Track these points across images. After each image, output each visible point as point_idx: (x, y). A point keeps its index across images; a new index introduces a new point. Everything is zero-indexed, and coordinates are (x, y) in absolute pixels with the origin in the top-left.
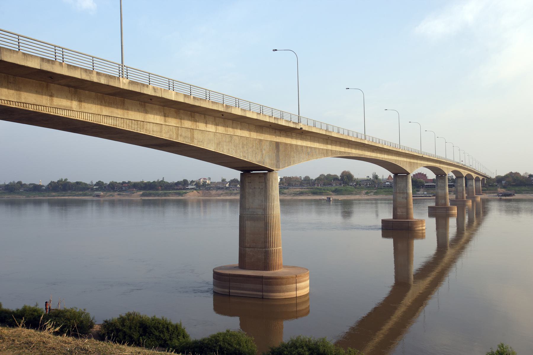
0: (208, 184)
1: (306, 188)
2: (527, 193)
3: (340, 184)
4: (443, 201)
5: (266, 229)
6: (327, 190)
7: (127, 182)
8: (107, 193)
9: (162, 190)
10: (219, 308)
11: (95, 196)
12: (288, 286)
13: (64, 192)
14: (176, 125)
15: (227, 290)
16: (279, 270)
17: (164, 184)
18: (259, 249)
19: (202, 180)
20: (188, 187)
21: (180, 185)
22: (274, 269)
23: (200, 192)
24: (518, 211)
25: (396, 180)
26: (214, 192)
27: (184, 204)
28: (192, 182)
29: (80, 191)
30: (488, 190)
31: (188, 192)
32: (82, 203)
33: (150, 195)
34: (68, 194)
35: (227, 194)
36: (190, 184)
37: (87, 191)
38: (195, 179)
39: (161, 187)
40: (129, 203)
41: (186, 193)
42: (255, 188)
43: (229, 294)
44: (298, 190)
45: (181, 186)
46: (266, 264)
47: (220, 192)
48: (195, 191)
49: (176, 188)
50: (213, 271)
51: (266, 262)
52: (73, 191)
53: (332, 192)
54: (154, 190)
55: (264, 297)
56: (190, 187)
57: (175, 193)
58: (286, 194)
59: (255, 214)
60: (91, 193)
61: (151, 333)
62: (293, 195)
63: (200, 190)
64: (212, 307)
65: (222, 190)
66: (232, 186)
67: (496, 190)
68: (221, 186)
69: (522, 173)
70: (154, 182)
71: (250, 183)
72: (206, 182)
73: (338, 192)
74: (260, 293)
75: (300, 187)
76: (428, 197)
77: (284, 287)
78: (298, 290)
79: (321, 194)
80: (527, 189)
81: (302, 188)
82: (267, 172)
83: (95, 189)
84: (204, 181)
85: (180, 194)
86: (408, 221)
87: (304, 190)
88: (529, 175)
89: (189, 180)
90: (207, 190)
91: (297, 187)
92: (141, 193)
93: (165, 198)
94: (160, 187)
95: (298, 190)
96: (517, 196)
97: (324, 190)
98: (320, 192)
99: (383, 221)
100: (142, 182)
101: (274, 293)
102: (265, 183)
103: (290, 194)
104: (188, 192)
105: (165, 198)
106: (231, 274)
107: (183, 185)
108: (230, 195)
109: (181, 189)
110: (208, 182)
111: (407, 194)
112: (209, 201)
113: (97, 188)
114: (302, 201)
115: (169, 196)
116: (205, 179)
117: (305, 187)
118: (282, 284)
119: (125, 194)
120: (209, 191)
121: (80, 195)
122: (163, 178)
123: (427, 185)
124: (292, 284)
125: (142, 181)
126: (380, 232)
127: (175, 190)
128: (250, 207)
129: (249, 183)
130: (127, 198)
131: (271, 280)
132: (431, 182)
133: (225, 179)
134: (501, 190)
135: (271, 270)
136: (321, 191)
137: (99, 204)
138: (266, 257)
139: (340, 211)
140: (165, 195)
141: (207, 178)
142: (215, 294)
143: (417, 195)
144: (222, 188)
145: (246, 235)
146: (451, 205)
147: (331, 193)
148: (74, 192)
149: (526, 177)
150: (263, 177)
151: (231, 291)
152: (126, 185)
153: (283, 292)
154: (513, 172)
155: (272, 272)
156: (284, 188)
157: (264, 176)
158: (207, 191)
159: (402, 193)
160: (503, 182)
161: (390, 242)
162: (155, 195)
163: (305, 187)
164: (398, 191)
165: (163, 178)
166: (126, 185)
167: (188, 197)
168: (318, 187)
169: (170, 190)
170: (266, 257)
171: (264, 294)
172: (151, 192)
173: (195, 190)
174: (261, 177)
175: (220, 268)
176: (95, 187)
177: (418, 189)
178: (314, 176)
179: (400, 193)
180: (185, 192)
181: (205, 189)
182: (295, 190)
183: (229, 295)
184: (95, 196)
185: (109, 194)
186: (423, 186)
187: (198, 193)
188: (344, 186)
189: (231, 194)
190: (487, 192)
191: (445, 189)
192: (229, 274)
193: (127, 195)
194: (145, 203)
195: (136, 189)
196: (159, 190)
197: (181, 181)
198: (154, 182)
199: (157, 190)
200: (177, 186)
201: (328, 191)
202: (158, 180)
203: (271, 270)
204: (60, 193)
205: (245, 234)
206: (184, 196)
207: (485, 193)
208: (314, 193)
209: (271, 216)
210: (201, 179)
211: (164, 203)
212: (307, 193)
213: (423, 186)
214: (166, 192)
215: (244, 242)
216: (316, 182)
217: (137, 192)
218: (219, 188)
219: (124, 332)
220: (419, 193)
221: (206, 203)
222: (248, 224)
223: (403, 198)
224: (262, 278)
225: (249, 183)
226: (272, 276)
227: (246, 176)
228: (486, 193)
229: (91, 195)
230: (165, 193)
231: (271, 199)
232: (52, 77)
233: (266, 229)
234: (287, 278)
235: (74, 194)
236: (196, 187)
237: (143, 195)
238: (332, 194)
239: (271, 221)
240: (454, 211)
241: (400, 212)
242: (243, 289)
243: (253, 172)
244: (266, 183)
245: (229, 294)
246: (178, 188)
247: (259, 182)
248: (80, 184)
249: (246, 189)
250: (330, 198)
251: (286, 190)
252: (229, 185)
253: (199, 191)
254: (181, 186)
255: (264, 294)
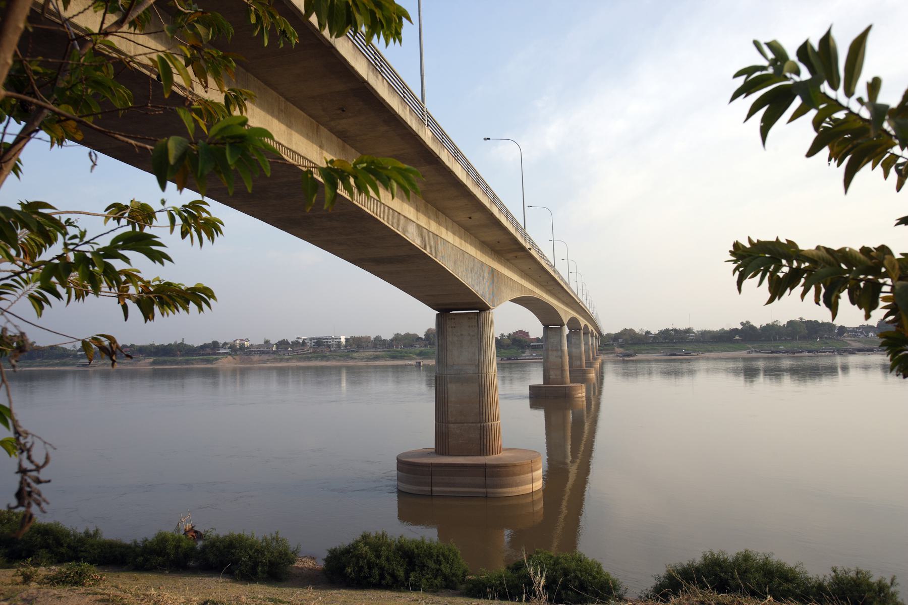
0: (248, 348)
1: (382, 350)
2: (648, 353)
3: (426, 346)
4: (579, 363)
5: (481, 395)
6: (410, 353)
7: (129, 345)
8: (98, 361)
9: (182, 355)
10: (406, 515)
11: (81, 366)
12: (523, 476)
13: (30, 361)
14: (424, 226)
15: (428, 489)
16: (499, 454)
17: (184, 348)
18: (470, 425)
19: (238, 342)
20: (219, 351)
21: (207, 349)
22: (494, 453)
23: (237, 358)
24: (636, 374)
25: (548, 334)
26: (256, 358)
27: (212, 374)
28: (225, 344)
29: (56, 359)
30: (604, 350)
31: (219, 359)
32: (61, 375)
33: (164, 363)
34: (38, 364)
35: (275, 360)
36: (222, 347)
37: (67, 359)
38: (230, 340)
39: (180, 352)
40: (133, 375)
41: (217, 359)
42: (462, 335)
43: (430, 494)
44: (371, 353)
45: (208, 351)
46: (482, 447)
47: (266, 357)
48: (229, 357)
49: (201, 352)
50: (397, 459)
51: (482, 443)
52: (45, 359)
53: (415, 355)
54: (170, 356)
55: (488, 495)
56: (221, 351)
57: (201, 359)
58: (356, 359)
59: (463, 373)
60: (74, 362)
61: (423, 566)
62: (365, 360)
63: (237, 355)
64: (396, 514)
65: (268, 355)
66: (281, 349)
67: (613, 349)
68: (266, 350)
69: (637, 330)
70: (170, 345)
71: (454, 327)
72: (244, 344)
73: (423, 355)
74: (483, 490)
75: (374, 350)
76: (538, 359)
77: (517, 478)
78: (535, 482)
79: (402, 358)
80: (648, 348)
81: (376, 350)
82: (478, 311)
83: (79, 356)
84: (241, 342)
85: (208, 361)
86: (565, 387)
87: (380, 353)
88: (646, 332)
89: (221, 341)
90: (246, 356)
91: (370, 350)
92: (151, 360)
93: (188, 366)
94: (178, 352)
95: (371, 353)
96: (639, 357)
97: (406, 353)
98: (401, 356)
99: (532, 388)
100: (152, 346)
101: (504, 487)
102: (478, 327)
103: (362, 359)
104: (219, 359)
105: (188, 366)
106: (434, 464)
107: (212, 349)
108: (280, 362)
109: (209, 354)
110: (247, 344)
111: (562, 351)
112: (249, 369)
113: (82, 354)
114: (376, 367)
115: (193, 364)
116: (242, 340)
117: (379, 350)
118: (514, 474)
119: (127, 362)
120: (250, 356)
121: (57, 365)
122: (183, 339)
123: (533, 345)
124: (527, 473)
125: (152, 343)
126: (527, 402)
127: (201, 356)
128: (455, 363)
129: (453, 328)
130: (130, 367)
131: (498, 470)
132: (535, 342)
133: (269, 341)
134: (619, 350)
135: (490, 455)
136: (402, 354)
137: (85, 376)
138: (482, 436)
139: (424, 378)
140: (187, 362)
141: (244, 339)
142: (401, 493)
143: (522, 358)
144: (268, 353)
145: (449, 405)
146: (586, 367)
147: (415, 356)
148: (46, 361)
149: (641, 335)
150: (475, 318)
151: (434, 489)
152: (128, 349)
153: (516, 486)
154: (628, 328)
155: (492, 457)
156: (353, 351)
157: (476, 317)
158: (247, 357)
159: (556, 350)
160: (620, 340)
161: (540, 414)
162: (172, 363)
163: (379, 350)
164: (550, 348)
165: (183, 339)
166: (128, 349)
167: (221, 364)
168: (397, 349)
169: (193, 356)
170: (482, 436)
171: (488, 490)
172: (166, 358)
173: (230, 355)
174: (472, 318)
175: (406, 454)
176: (79, 353)
177: (523, 350)
178: (388, 336)
179: (552, 350)
180: (216, 358)
181: (244, 354)
182: (367, 353)
183: (431, 495)
184: (81, 366)
185: (103, 362)
186: (529, 346)
187: (234, 360)
188: (430, 347)
189: (281, 360)
190: (604, 352)
191: (580, 347)
192: (431, 463)
193: (130, 364)
194: (157, 375)
195: (142, 354)
196: (177, 356)
197: (210, 344)
198: (169, 344)
199: (175, 355)
200: (203, 350)
201: (411, 355)
202: (175, 343)
203: (490, 455)
204: (24, 362)
205: (447, 403)
206: (215, 364)
207: (602, 353)
208: (394, 357)
209: (488, 375)
210: (236, 340)
211: (184, 374)
212: (383, 357)
213: (529, 346)
214: (187, 358)
215: (446, 415)
216: (394, 343)
217: (144, 359)
218: (263, 353)
219: (382, 568)
220: (525, 355)
221: (243, 372)
222: (452, 388)
223: (556, 357)
224: (485, 466)
225: (453, 328)
226: (495, 463)
227: (447, 318)
228: (603, 354)
229: (73, 365)
230: (188, 360)
231: (487, 351)
232: (345, 109)
233: (481, 395)
234: (521, 465)
235: (47, 364)
236: (231, 351)
237: (154, 363)
238: (417, 358)
239: (488, 384)
240: (592, 375)
241: (553, 375)
242: (454, 485)
243: (453, 312)
244: (479, 328)
245: (430, 494)
246: (206, 352)
247: (469, 327)
248: (55, 349)
249: (448, 337)
250: (420, 363)
251: (355, 354)
252: (277, 348)
253: (234, 357)
254: (208, 351)
255: (488, 490)
